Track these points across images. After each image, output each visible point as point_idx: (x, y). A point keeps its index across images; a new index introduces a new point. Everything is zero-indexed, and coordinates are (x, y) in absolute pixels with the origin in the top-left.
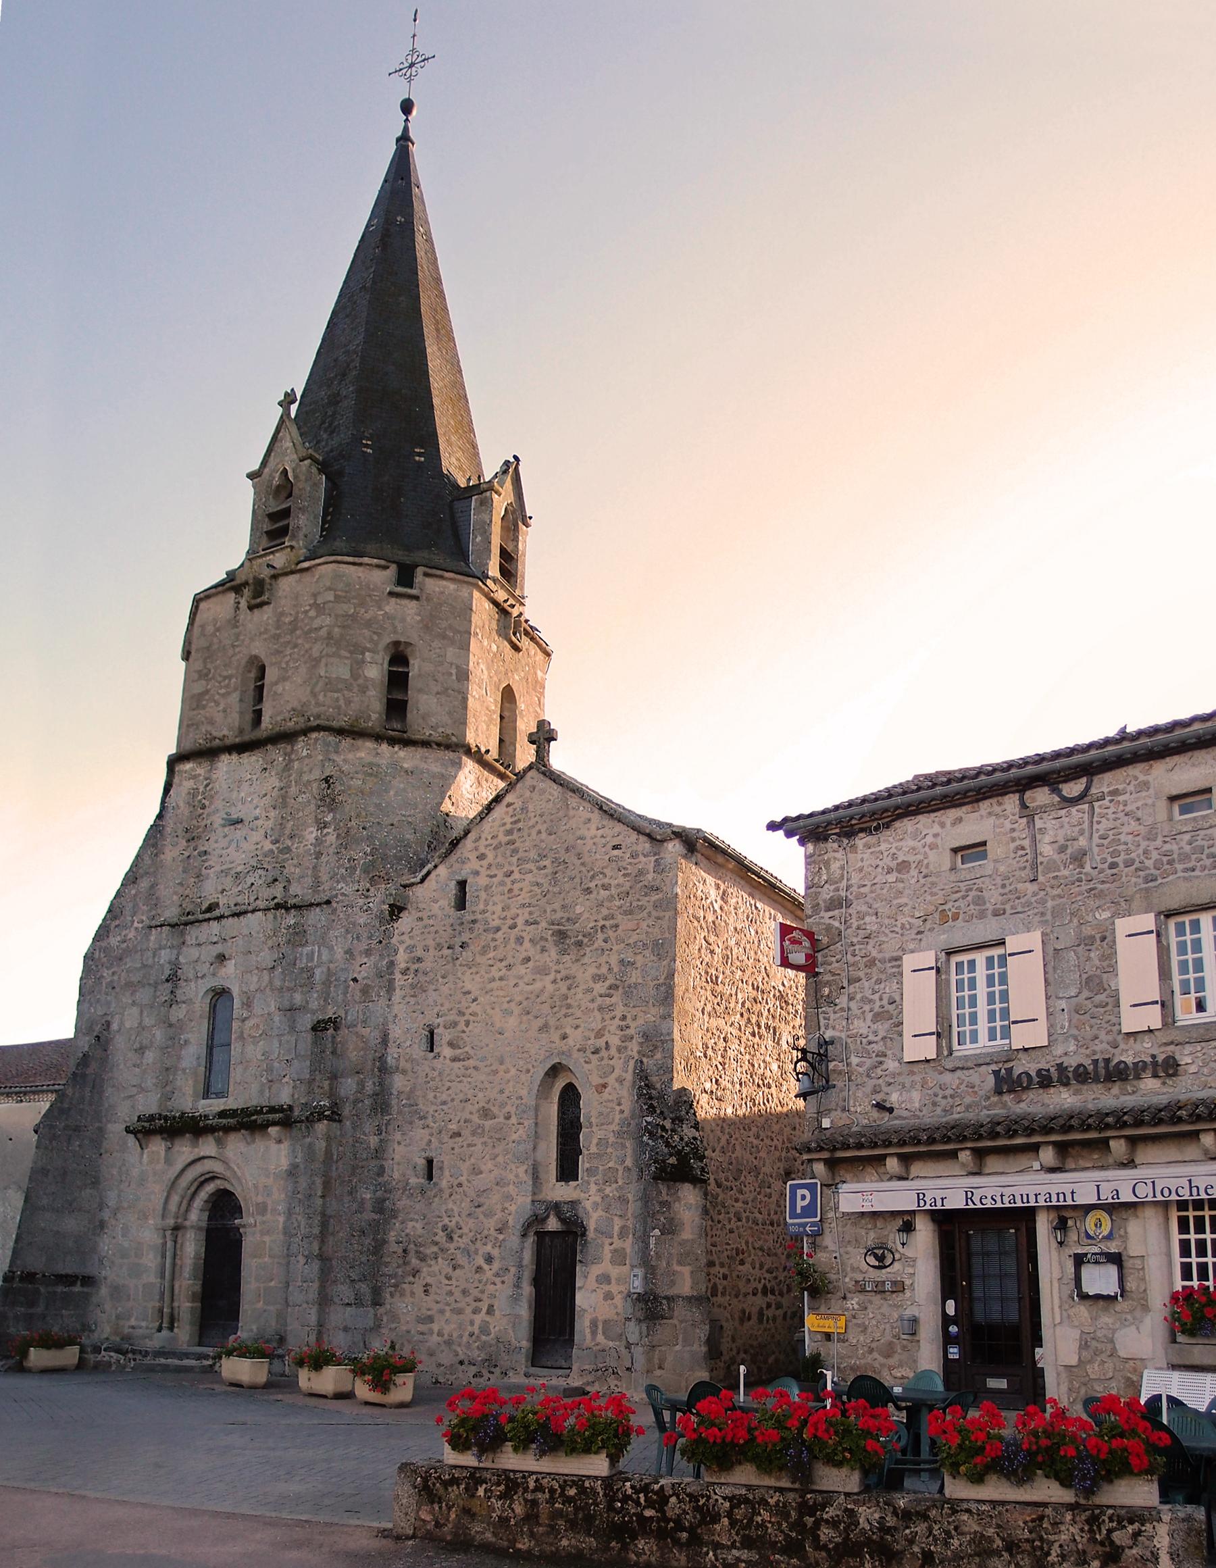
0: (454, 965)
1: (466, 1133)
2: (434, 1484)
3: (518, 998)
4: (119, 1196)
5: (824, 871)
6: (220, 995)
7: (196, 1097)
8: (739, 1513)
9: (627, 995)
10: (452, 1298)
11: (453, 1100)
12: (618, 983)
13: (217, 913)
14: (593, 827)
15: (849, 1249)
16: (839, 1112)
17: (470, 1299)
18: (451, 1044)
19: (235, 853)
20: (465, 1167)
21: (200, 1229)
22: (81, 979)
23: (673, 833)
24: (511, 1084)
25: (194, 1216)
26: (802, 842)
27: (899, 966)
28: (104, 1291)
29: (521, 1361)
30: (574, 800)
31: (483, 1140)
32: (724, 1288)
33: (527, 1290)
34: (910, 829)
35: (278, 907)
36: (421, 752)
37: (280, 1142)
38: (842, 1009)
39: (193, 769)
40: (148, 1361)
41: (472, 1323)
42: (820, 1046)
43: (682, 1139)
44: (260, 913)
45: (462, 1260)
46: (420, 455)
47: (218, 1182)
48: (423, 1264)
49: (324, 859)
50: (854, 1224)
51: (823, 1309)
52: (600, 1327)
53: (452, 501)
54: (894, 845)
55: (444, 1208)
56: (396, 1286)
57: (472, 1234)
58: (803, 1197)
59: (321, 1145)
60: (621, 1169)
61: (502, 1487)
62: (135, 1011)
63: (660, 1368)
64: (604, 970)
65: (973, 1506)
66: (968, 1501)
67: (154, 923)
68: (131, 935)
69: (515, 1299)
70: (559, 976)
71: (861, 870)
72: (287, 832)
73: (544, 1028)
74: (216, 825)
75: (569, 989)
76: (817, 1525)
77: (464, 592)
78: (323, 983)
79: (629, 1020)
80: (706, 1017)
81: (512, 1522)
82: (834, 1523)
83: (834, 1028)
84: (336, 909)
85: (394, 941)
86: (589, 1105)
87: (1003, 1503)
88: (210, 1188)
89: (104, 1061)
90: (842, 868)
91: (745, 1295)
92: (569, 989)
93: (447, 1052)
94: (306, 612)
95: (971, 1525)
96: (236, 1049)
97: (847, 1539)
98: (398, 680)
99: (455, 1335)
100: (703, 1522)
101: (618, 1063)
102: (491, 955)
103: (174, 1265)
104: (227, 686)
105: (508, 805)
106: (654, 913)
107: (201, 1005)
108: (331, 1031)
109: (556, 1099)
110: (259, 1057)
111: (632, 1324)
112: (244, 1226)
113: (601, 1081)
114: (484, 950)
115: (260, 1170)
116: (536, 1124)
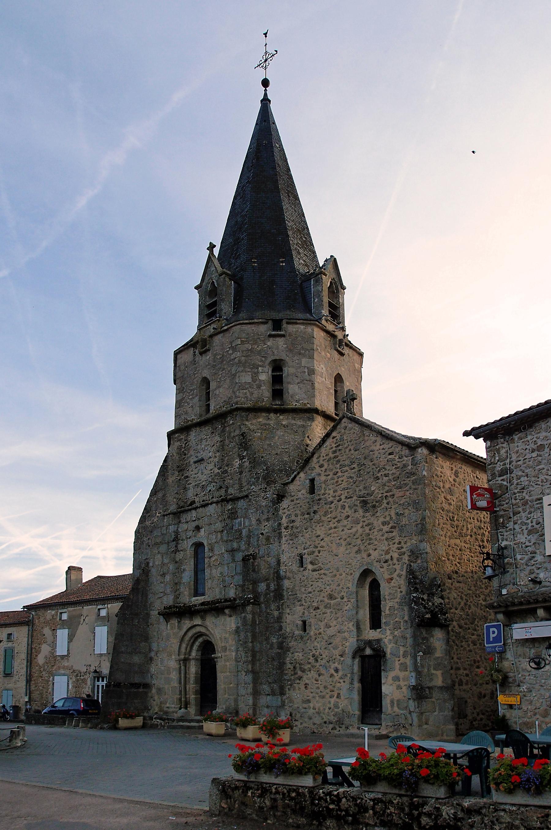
0: (311, 523)
1: (321, 607)
2: (227, 789)
3: (344, 537)
4: (158, 645)
5: (497, 455)
6: (199, 546)
7: (190, 596)
8: (378, 807)
9: (401, 531)
10: (319, 691)
11: (314, 591)
12: (395, 525)
13: (194, 506)
14: (378, 444)
15: (521, 659)
16: (511, 585)
17: (328, 691)
18: (311, 563)
19: (201, 474)
20: (322, 625)
21: (197, 659)
22: (134, 543)
23: (421, 443)
24: (343, 581)
25: (194, 654)
26: (485, 441)
27: (542, 503)
28: (154, 691)
29: (355, 721)
30: (367, 432)
31: (330, 610)
32: (467, 681)
33: (357, 685)
34: (543, 426)
35: (223, 500)
36: (291, 416)
37: (230, 616)
38: (510, 530)
39: (179, 436)
40: (175, 724)
41: (330, 702)
42: (499, 550)
43: (433, 604)
44: (214, 505)
45: (323, 671)
46: (282, 262)
47: (204, 637)
48: (304, 674)
49: (244, 474)
50: (523, 645)
51: (507, 692)
52: (395, 703)
53: (302, 283)
54: (535, 436)
55: (313, 645)
56: (291, 685)
57: (328, 658)
58: (494, 632)
59: (249, 617)
60: (402, 621)
61: (260, 792)
62: (159, 556)
63: (426, 724)
64: (388, 519)
65: (507, 807)
66: (506, 804)
67: (166, 513)
68: (155, 520)
69: (351, 690)
70: (365, 524)
71: (517, 452)
72: (225, 462)
73: (358, 551)
74: (191, 463)
75: (370, 530)
76: (420, 815)
77: (309, 329)
78: (247, 537)
79: (402, 544)
80: (447, 539)
81: (265, 809)
82: (429, 815)
83: (507, 540)
84: (251, 499)
85: (280, 513)
86: (385, 589)
87: (527, 806)
88: (200, 640)
89: (147, 581)
90: (507, 452)
91: (481, 685)
92: (370, 530)
93: (310, 567)
94: (228, 351)
95: (506, 818)
96: (207, 572)
97: (436, 824)
98: (277, 379)
99: (321, 709)
100: (359, 812)
101: (397, 567)
102: (329, 516)
103: (185, 677)
104: (193, 394)
105: (334, 438)
106: (413, 487)
107: (190, 552)
108: (252, 560)
109: (367, 587)
110: (219, 575)
111: (411, 702)
112: (216, 658)
113: (389, 577)
114: (326, 514)
115: (223, 630)
116: (357, 601)
